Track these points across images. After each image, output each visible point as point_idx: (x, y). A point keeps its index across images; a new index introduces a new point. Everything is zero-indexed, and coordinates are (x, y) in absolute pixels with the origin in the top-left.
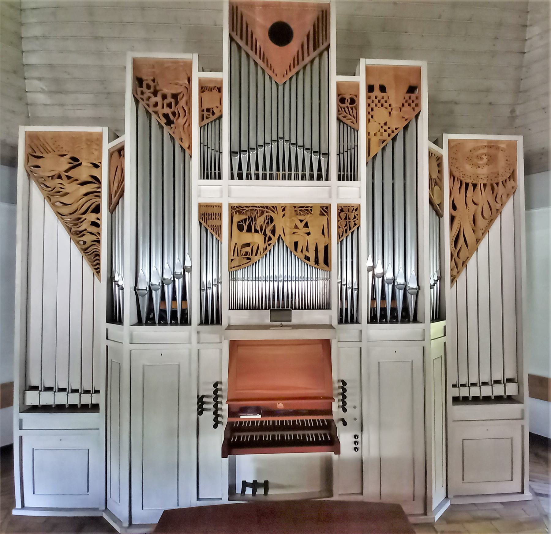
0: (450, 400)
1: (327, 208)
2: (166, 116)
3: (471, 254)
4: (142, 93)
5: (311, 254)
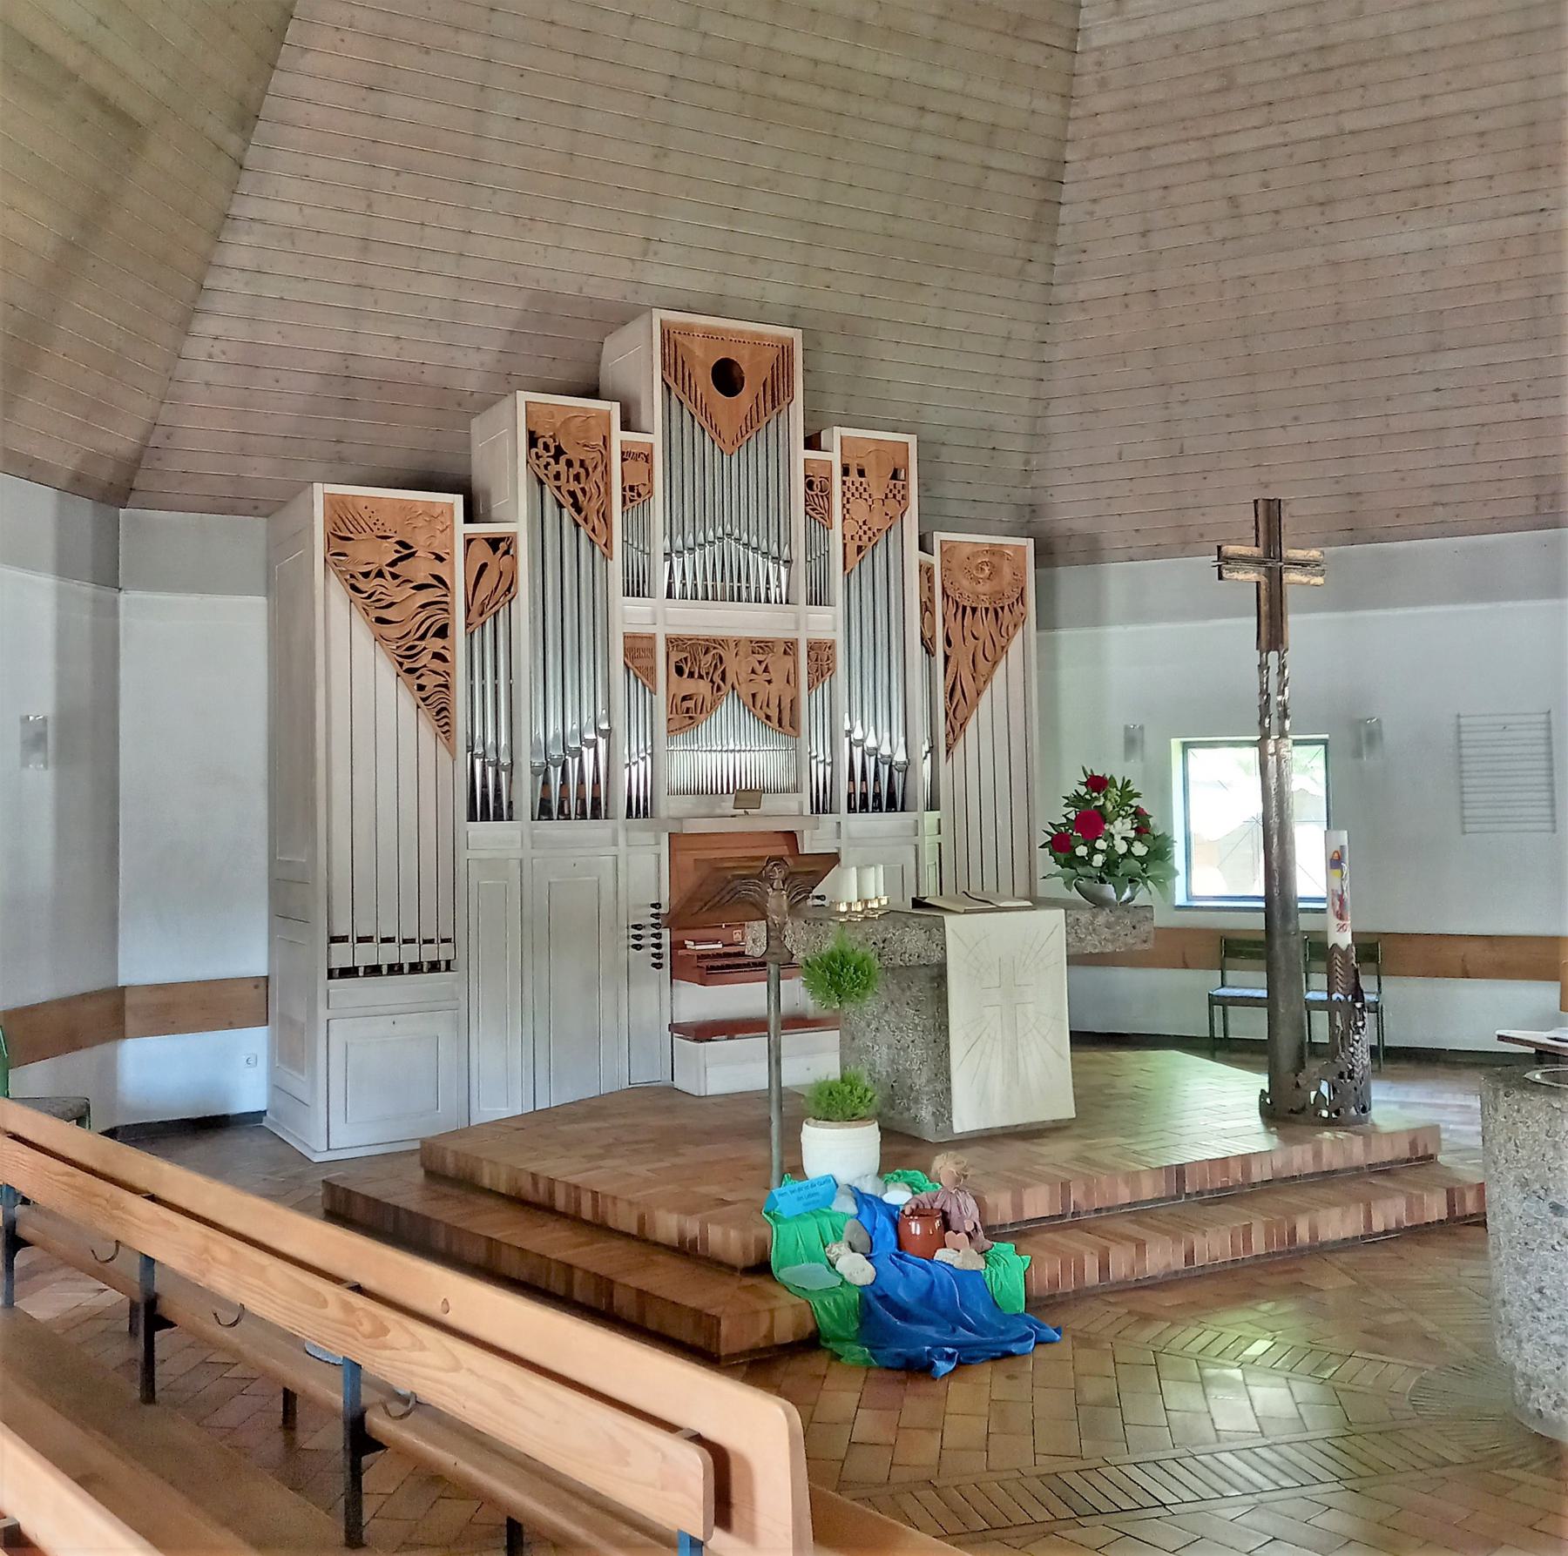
3: (970, 713)
5: (774, 714)
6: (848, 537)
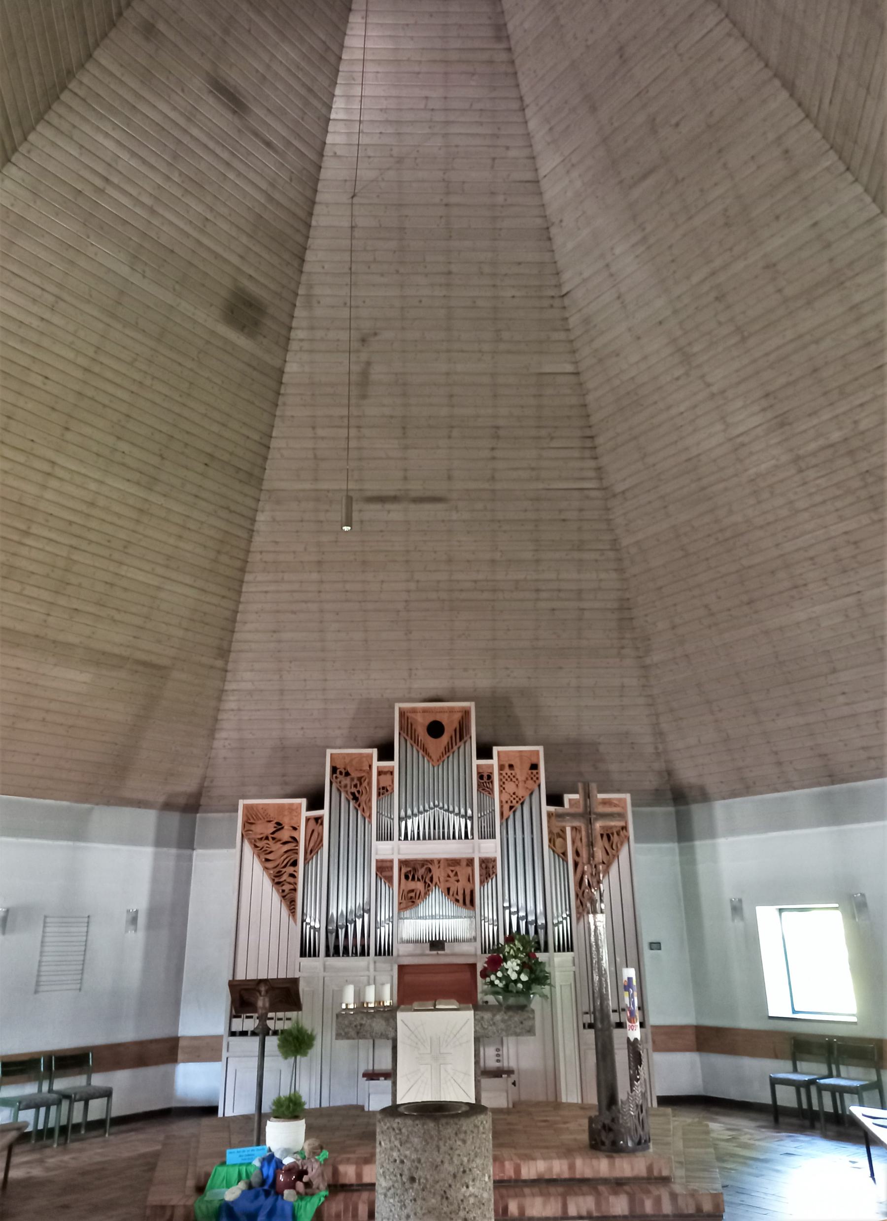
0: (581, 1026)
2: (353, 794)
5: (460, 898)
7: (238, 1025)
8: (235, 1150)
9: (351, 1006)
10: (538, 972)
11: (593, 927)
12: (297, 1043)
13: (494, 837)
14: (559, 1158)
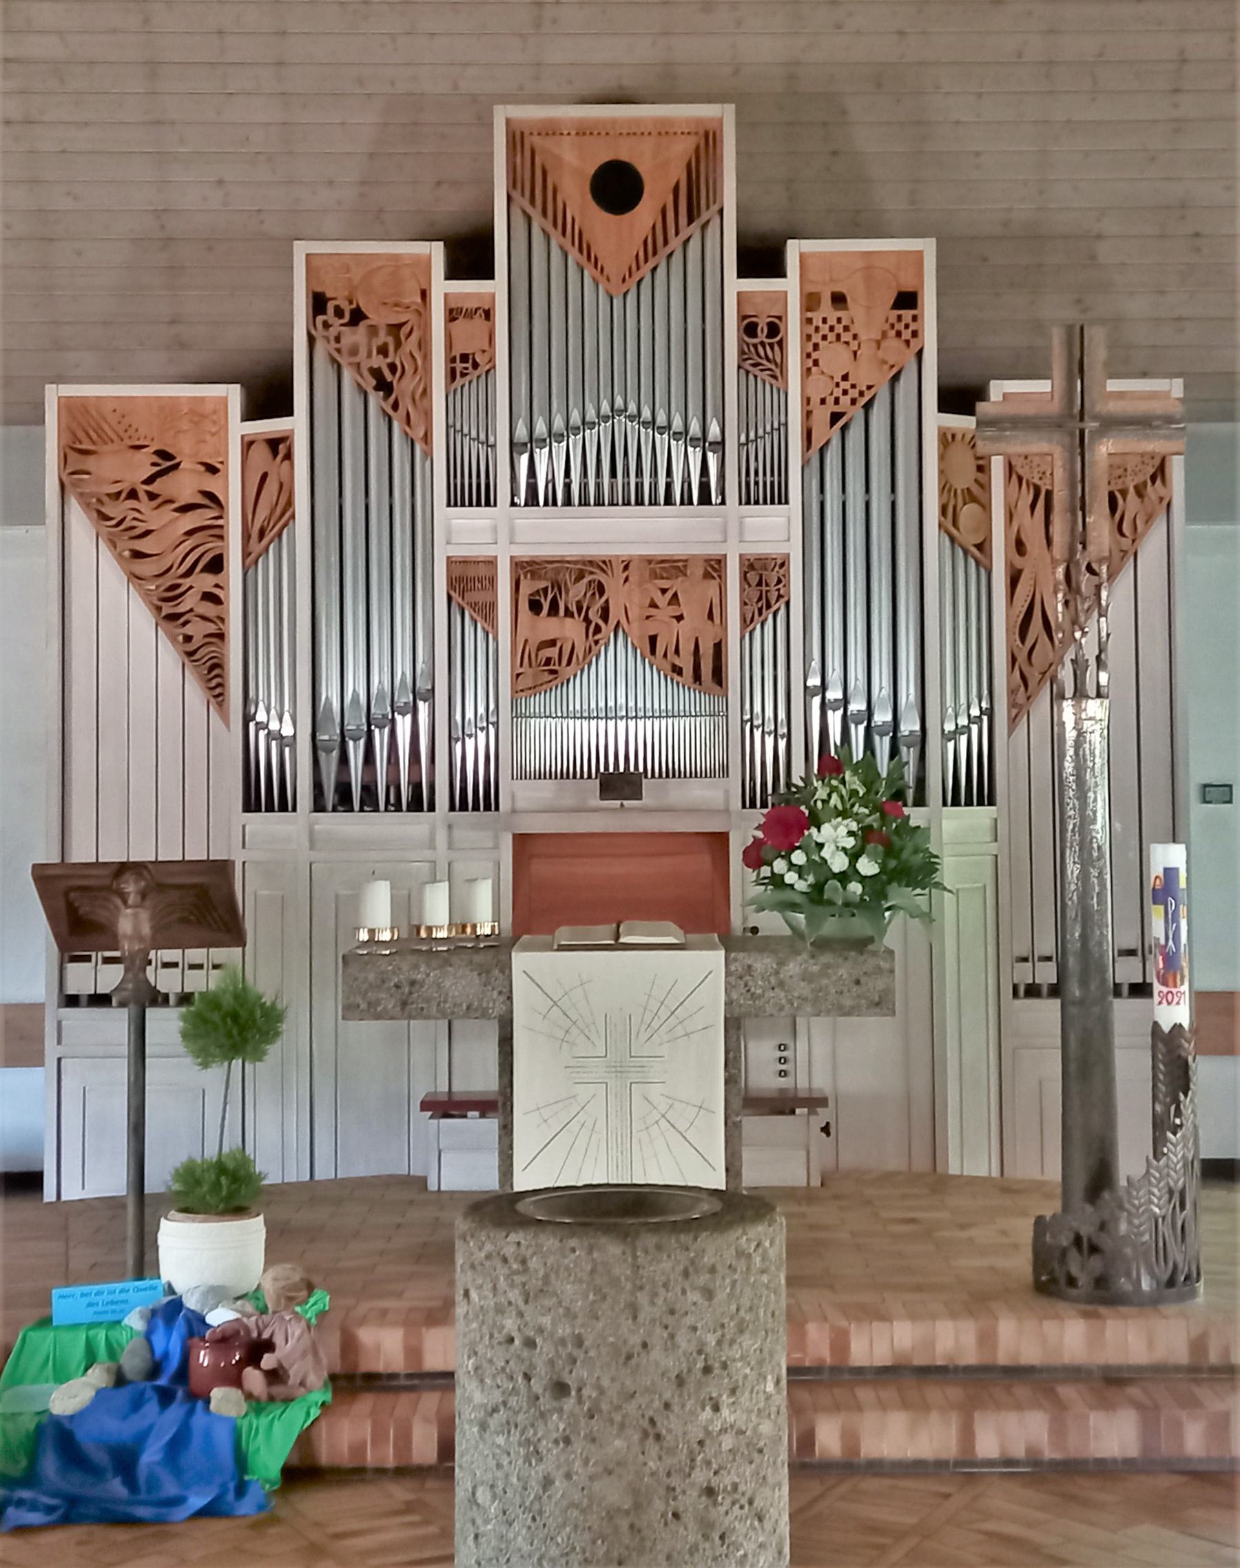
0: (1007, 991)
1: (719, 562)
2: (376, 373)
4: (326, 325)
5: (686, 662)
6: (815, 400)
7: (81, 978)
8: (77, 1290)
9: (386, 936)
10: (905, 855)
11: (1070, 735)
12: (234, 1028)
13: (784, 500)
14: (953, 1315)
